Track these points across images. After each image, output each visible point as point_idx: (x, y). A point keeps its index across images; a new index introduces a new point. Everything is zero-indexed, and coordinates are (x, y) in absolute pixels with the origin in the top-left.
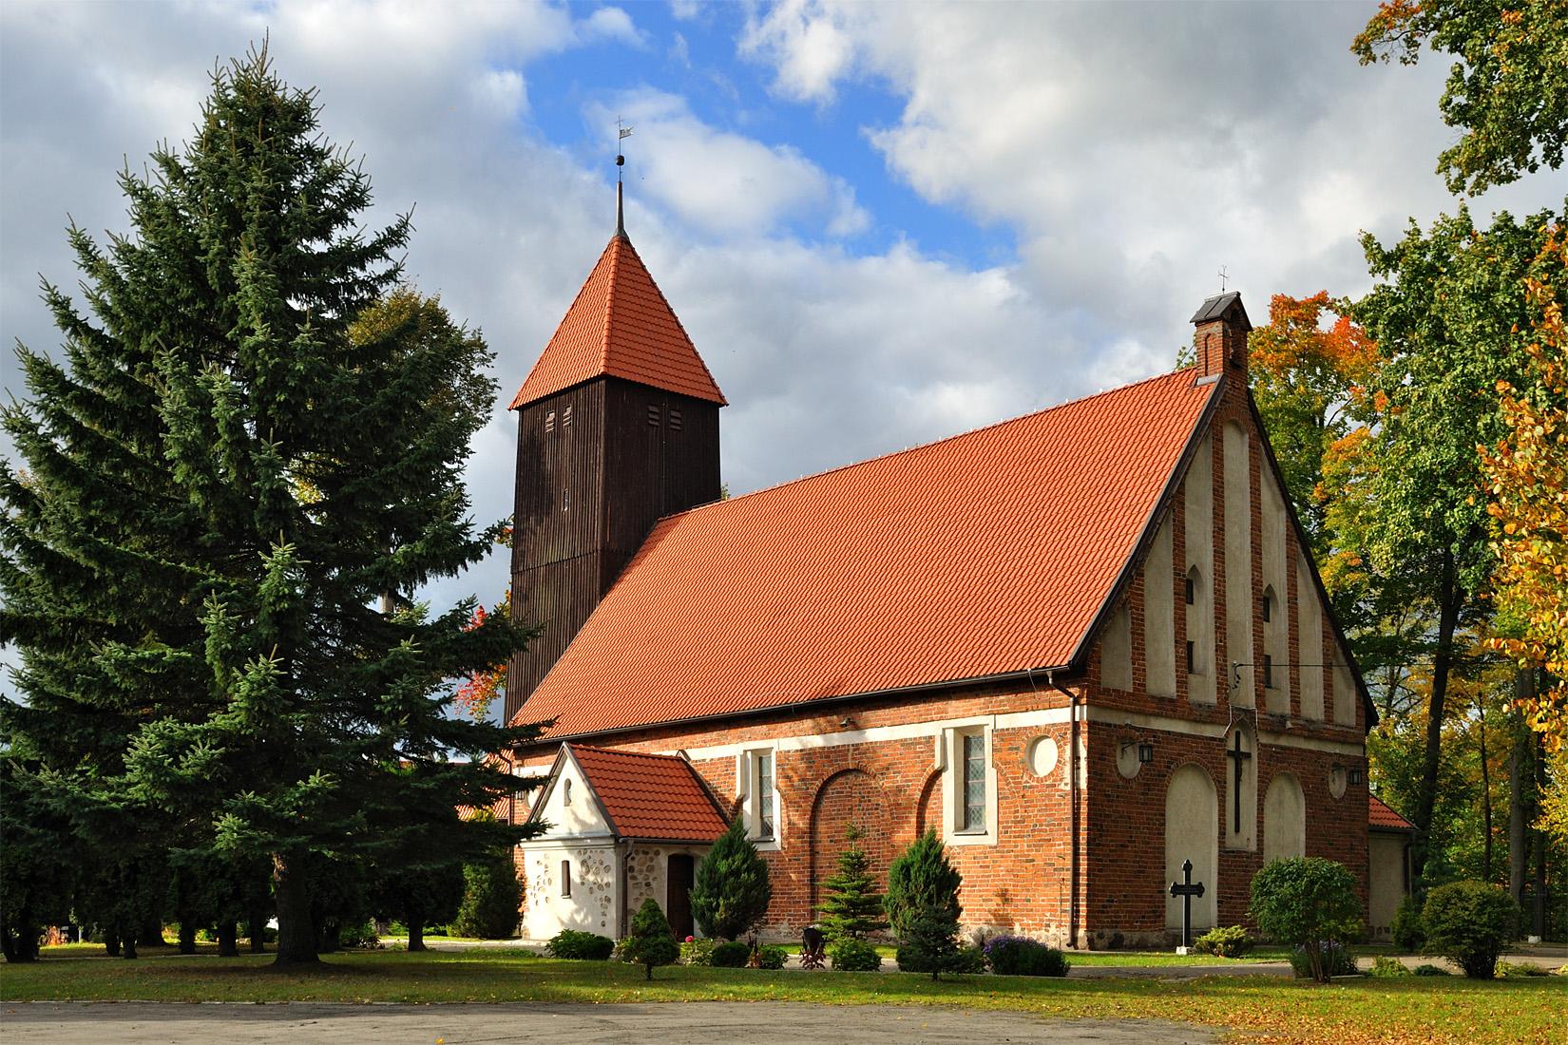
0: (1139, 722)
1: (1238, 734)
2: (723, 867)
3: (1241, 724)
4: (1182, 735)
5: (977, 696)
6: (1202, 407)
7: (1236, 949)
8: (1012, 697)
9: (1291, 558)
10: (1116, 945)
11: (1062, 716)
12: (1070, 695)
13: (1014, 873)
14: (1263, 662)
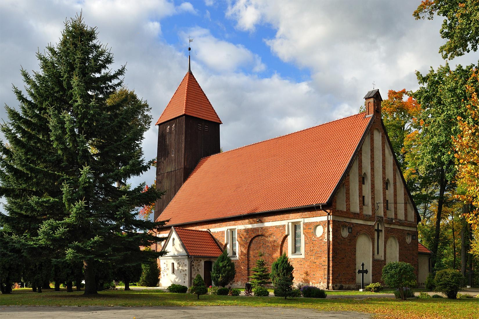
0: (348, 220)
1: (378, 224)
2: (221, 265)
3: (379, 221)
4: (361, 224)
5: (299, 212)
6: (367, 124)
7: (378, 290)
8: (309, 213)
9: (394, 170)
10: (341, 288)
11: (325, 218)
12: (327, 212)
13: (310, 267)
14: (386, 202)
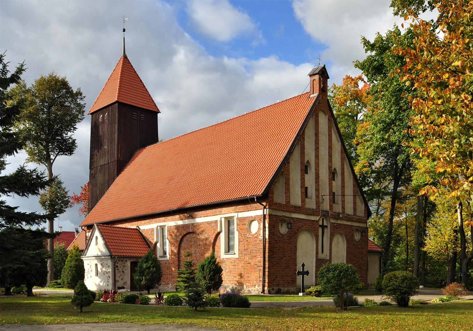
0: (287, 214)
1: (323, 219)
2: (144, 266)
3: (324, 216)
4: (303, 219)
5: (232, 206)
6: (311, 105)
7: (319, 294)
8: (243, 206)
9: (342, 159)
10: (279, 292)
11: (260, 212)
12: (263, 205)
13: (242, 268)
14: (332, 195)
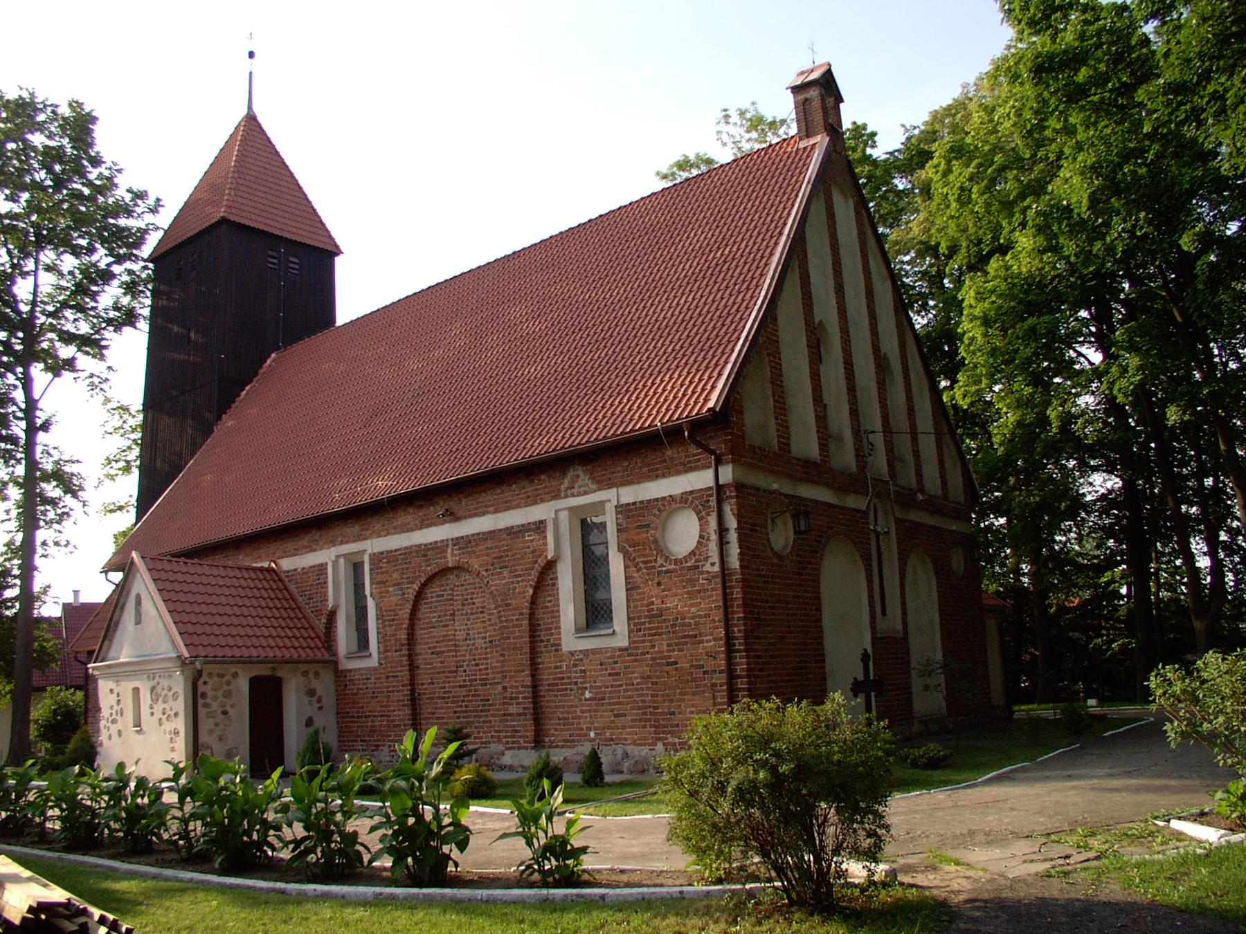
11: (702, 479)
12: (712, 452)
